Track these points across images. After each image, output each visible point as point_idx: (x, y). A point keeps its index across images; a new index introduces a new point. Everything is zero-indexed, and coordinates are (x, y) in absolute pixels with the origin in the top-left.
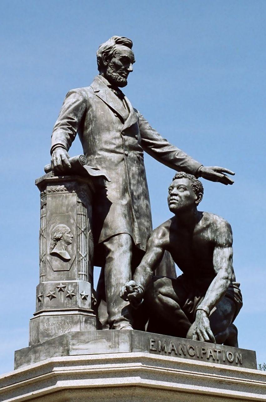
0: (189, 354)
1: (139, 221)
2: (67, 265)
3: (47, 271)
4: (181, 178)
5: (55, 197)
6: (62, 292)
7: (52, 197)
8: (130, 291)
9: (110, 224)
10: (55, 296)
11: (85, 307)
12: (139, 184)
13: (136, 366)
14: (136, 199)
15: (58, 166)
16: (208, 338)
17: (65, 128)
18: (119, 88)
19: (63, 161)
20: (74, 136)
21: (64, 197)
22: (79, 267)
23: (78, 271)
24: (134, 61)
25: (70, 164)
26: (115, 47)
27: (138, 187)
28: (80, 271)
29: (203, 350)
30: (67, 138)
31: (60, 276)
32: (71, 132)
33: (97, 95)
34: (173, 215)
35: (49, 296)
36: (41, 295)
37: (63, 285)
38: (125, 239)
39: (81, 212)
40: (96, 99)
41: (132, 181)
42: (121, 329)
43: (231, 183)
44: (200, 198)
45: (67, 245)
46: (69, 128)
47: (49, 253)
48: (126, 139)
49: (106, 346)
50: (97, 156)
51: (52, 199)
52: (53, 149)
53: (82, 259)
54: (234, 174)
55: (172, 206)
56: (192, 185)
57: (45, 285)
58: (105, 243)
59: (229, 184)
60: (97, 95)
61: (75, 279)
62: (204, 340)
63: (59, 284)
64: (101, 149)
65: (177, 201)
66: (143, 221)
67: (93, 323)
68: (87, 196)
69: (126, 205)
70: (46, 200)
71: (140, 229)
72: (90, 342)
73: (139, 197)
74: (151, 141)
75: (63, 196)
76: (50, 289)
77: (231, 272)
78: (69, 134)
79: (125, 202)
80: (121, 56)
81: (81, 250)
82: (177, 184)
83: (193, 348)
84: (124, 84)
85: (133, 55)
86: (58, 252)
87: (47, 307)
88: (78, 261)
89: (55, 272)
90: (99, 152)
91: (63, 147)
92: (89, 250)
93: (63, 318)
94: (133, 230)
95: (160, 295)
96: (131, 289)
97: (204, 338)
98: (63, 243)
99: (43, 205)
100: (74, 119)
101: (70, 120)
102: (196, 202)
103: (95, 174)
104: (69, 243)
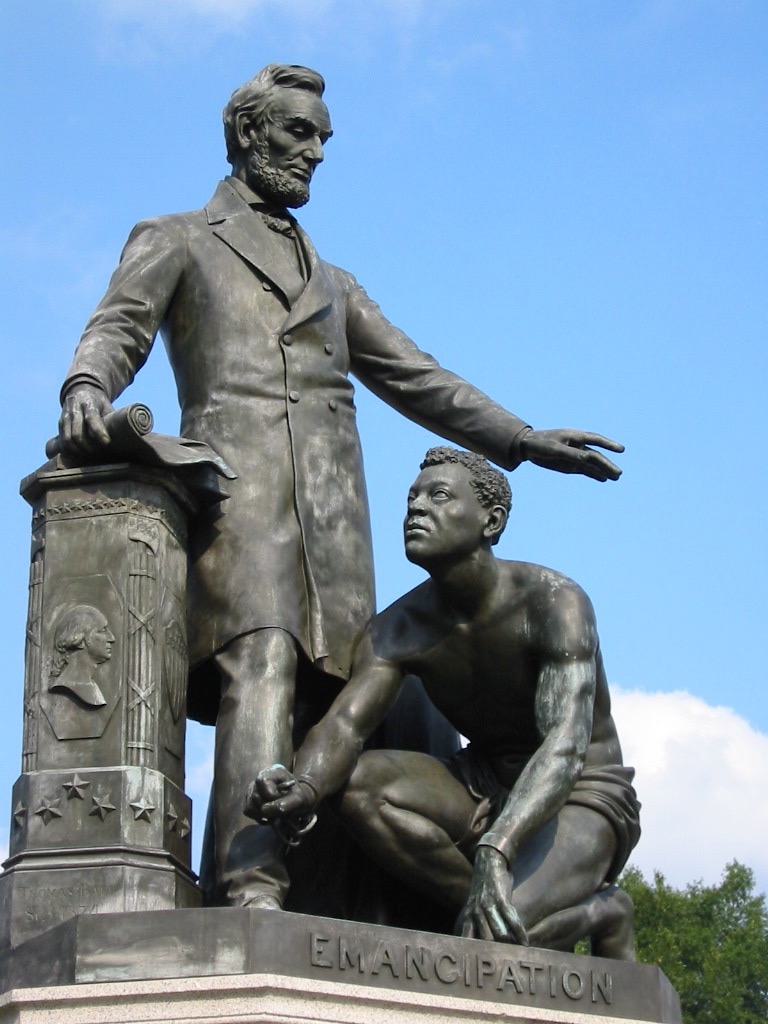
0: (438, 977)
1: (329, 592)
2: (95, 723)
3: (41, 742)
4: (441, 462)
5: (69, 529)
6: (77, 799)
7: (60, 528)
8: (269, 794)
9: (233, 603)
10: (59, 813)
11: (144, 843)
12: (331, 486)
13: (251, 1014)
14: (320, 528)
15: (74, 438)
16: (503, 930)
17: (114, 329)
18: (289, 209)
19: (86, 424)
20: (142, 351)
21: (93, 528)
22: (130, 728)
23: (127, 740)
24: (329, 131)
25: (105, 432)
26: (271, 94)
27: (329, 495)
28: (133, 740)
29: (487, 964)
30: (114, 358)
31: (75, 754)
32: (130, 341)
33: (214, 233)
34: (421, 575)
35: (41, 814)
36: (21, 809)
37: (83, 780)
38: (276, 647)
39: (141, 568)
40: (211, 243)
41: (310, 478)
42: (245, 905)
43: (613, 475)
44: (498, 522)
45: (96, 666)
46: (125, 330)
47: (45, 688)
48: (293, 356)
49: (179, 956)
50: (209, 409)
51: (60, 534)
52: (68, 387)
53: (139, 704)
54: (620, 450)
55: (413, 544)
56: (474, 482)
57: (31, 779)
58: (219, 657)
59: (608, 480)
60: (214, 233)
61: (118, 764)
62: (492, 937)
63: (71, 777)
64: (222, 387)
65: (428, 530)
66: (343, 592)
67: (166, 890)
68: (161, 522)
69: (286, 546)
70: (44, 536)
71: (326, 615)
72: (135, 945)
73: (331, 524)
74: (384, 361)
75: (92, 523)
76: (46, 793)
77: (585, 735)
78: (126, 349)
79: (282, 537)
80: (287, 119)
81: (137, 677)
82: (428, 482)
83: (453, 958)
84: (299, 200)
85: (327, 115)
86: (71, 684)
87: (37, 844)
88: (127, 709)
89: (63, 744)
90: (215, 396)
91: (96, 383)
92: (165, 682)
93: (78, 876)
94: (306, 620)
95: (388, 809)
96: (271, 789)
97: (493, 931)
98: (87, 658)
99: (38, 551)
100: (143, 304)
101: (131, 307)
102: (487, 533)
103: (184, 459)
104: (101, 660)
